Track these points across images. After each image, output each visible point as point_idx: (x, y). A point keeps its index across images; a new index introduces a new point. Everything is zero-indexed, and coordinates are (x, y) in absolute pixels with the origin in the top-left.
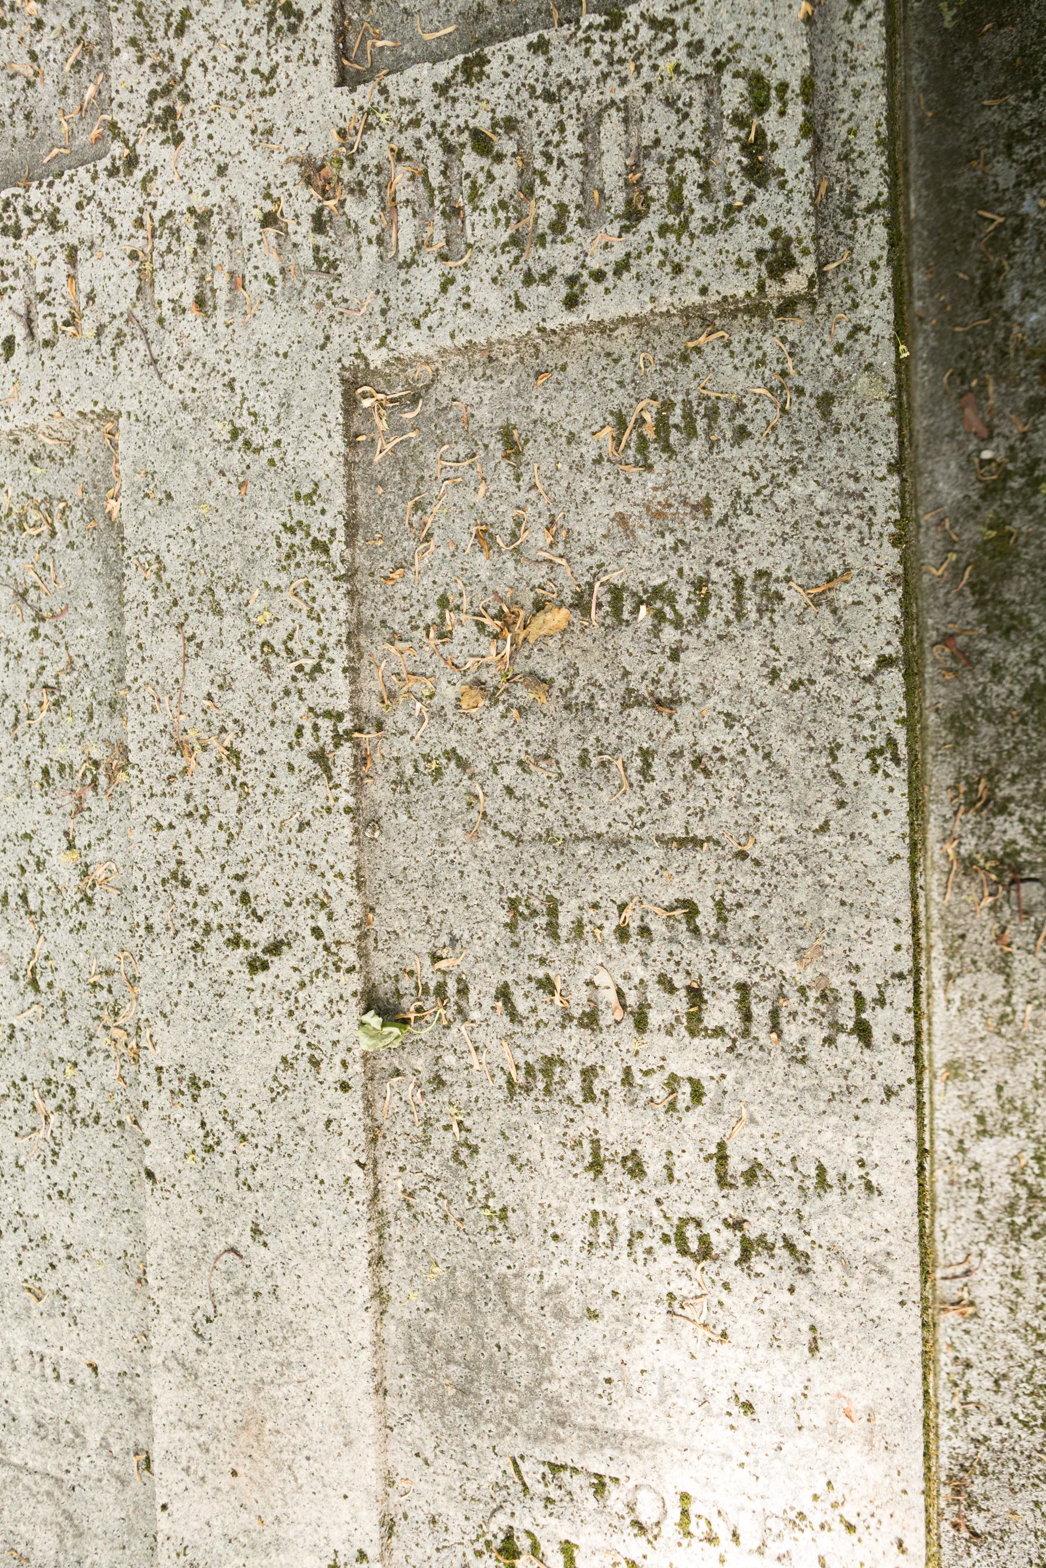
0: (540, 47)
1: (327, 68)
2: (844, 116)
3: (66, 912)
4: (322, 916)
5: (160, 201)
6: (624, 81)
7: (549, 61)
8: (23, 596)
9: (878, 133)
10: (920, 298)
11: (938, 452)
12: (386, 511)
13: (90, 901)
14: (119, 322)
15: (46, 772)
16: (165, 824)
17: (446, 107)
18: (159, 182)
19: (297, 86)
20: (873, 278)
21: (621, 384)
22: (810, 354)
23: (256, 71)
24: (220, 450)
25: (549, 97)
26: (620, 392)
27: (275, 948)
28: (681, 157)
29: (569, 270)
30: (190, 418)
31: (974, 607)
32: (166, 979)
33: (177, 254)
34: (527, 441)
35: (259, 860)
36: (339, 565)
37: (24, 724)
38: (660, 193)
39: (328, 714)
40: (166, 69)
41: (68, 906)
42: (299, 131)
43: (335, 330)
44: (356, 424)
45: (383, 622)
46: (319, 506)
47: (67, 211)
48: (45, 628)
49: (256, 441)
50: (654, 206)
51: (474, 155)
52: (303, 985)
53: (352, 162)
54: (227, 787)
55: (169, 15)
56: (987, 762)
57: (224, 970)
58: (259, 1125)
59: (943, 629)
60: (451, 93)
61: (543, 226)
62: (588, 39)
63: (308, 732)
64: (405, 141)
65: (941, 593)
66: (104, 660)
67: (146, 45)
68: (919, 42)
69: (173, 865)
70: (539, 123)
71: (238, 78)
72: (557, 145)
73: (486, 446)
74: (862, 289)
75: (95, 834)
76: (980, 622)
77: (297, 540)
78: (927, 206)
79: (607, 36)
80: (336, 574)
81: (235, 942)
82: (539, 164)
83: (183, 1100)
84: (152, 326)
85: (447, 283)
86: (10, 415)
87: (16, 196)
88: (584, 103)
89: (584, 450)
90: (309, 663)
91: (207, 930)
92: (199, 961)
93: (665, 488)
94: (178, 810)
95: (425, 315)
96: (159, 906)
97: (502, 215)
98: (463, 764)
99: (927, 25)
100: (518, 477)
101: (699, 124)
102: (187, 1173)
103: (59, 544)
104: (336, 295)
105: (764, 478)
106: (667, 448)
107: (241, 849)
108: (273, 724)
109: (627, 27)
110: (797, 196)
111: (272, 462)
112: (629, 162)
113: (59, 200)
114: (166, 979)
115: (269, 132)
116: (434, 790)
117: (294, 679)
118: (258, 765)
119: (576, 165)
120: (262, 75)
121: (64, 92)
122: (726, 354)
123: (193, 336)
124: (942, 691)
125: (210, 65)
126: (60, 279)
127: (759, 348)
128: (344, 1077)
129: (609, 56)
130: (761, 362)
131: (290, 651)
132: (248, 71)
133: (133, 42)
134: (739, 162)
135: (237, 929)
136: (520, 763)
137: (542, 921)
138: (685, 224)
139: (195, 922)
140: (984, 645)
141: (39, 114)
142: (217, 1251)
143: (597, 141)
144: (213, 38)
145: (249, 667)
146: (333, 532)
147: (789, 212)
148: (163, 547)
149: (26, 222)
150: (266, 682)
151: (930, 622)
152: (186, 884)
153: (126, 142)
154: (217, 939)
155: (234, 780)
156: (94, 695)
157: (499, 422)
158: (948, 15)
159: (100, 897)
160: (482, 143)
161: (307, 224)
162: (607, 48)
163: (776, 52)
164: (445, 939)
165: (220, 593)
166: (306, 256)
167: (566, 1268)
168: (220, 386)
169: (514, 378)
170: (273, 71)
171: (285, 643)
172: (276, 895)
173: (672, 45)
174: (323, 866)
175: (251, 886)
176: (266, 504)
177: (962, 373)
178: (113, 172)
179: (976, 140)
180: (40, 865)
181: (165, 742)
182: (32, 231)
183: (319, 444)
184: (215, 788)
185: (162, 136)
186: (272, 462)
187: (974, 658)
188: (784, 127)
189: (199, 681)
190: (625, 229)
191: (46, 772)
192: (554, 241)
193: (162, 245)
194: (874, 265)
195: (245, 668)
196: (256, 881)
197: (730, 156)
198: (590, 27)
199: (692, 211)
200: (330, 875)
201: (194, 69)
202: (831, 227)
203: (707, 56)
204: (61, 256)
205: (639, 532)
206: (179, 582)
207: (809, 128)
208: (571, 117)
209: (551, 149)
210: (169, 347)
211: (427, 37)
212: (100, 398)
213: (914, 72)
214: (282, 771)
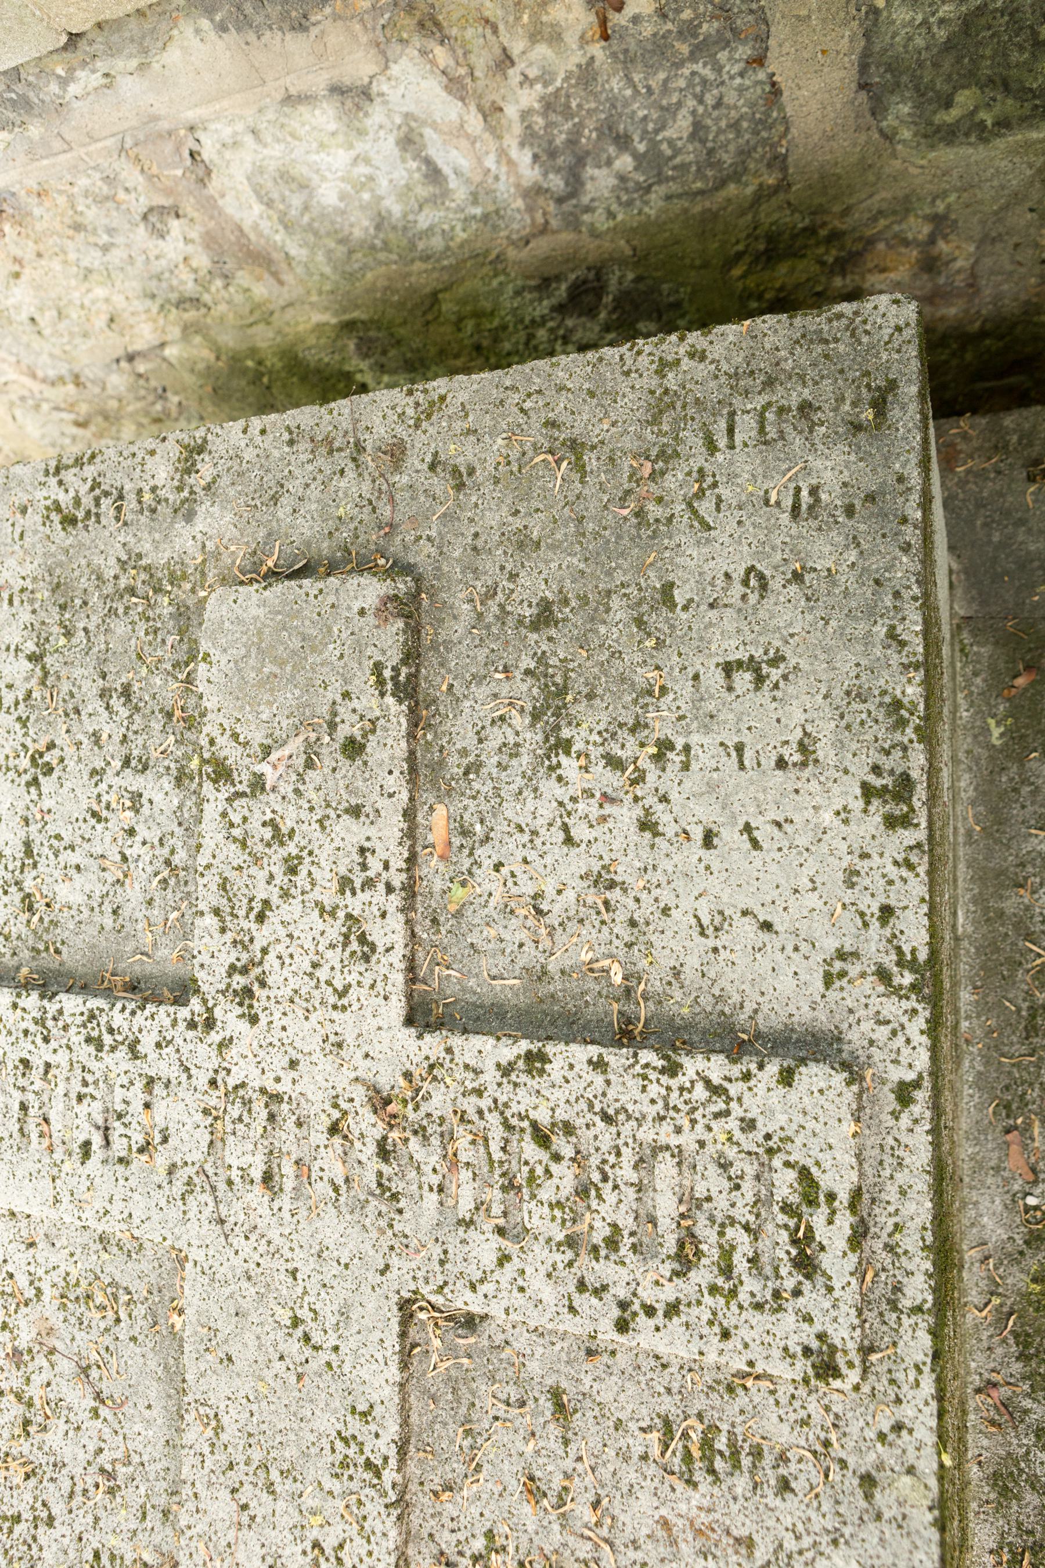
0: (599, 1065)
1: (397, 1008)
2: (891, 1209)
5: (234, 1069)
6: (678, 1130)
7: (608, 1082)
8: (85, 1370)
9: (923, 1239)
10: (968, 1017)
11: (982, 1183)
12: (437, 1426)
14: (190, 1171)
15: (97, 1555)
17: (508, 1088)
18: (233, 1052)
19: (368, 1012)
20: (917, 1381)
21: (669, 1391)
22: (854, 1429)
23: (329, 983)
25: (607, 1118)
26: (666, 1399)
28: (732, 1225)
29: (622, 1293)
30: (253, 1290)
31: (1018, 1359)
33: (247, 1125)
34: (576, 1411)
36: (391, 1492)
37: (79, 1499)
38: (711, 1251)
40: (245, 948)
42: (367, 1055)
43: (394, 1261)
44: (412, 1332)
45: (431, 1535)
46: (373, 1427)
47: (147, 1045)
49: (317, 1338)
50: (704, 1261)
51: (533, 1146)
53: (417, 1108)
55: (251, 900)
56: (1030, 1533)
59: (986, 1375)
60: (513, 1077)
61: (597, 1238)
62: (645, 1077)
64: (470, 1105)
65: (984, 1336)
66: (159, 1466)
67: (228, 918)
68: (968, 752)
70: (596, 1137)
71: (313, 983)
72: (613, 1167)
73: (536, 1400)
74: (905, 1388)
76: (1024, 1378)
77: (351, 1452)
78: (974, 922)
79: (665, 1079)
80: (388, 1501)
82: (596, 1177)
84: (222, 1186)
85: (504, 1259)
87: (102, 1010)
88: (640, 1135)
89: (631, 1441)
93: (709, 1511)
95: (482, 1281)
97: (557, 1213)
99: (975, 736)
100: (566, 1442)
101: (750, 1198)
103: (123, 1331)
104: (398, 1227)
105: (807, 1541)
106: (712, 1471)
109: (682, 1080)
110: (844, 1308)
112: (683, 1209)
113: (140, 1031)
115: (339, 1045)
119: (631, 1193)
120: (335, 990)
121: (150, 902)
122: (772, 1401)
123: (260, 1211)
124: (985, 1442)
125: (288, 961)
126: (137, 1106)
127: (803, 1407)
129: (666, 1099)
130: (804, 1423)
132: (323, 979)
133: (217, 912)
134: (788, 1253)
138: (733, 1293)
140: (1027, 1403)
141: (125, 912)
143: (651, 1171)
144: (290, 936)
146: (386, 1459)
147: (835, 1320)
148: (222, 1407)
149: (108, 1040)
151: (973, 1365)
153: (205, 1001)
157: (549, 1381)
158: (996, 732)
160: (542, 1139)
161: (372, 1148)
162: (664, 1092)
163: (825, 1158)
165: (275, 1475)
166: (371, 1179)
168: (282, 1269)
169: (565, 1345)
170: (347, 988)
171: (335, 1550)
173: (727, 1113)
176: (322, 1405)
177: (1007, 1106)
178: (192, 1025)
179: (1023, 865)
182: (113, 1049)
183: (375, 1366)
185: (239, 1011)
186: (329, 1364)
187: (1017, 1415)
188: (833, 1234)
190: (676, 1274)
191: (97, 1555)
192: (607, 1257)
193: (235, 1111)
194: (919, 1370)
197: (777, 1243)
198: (647, 1066)
199: (741, 1283)
201: (271, 958)
202: (876, 1312)
203: (759, 1135)
204: (139, 1084)
205: (683, 1545)
206: (235, 1446)
207: (858, 1238)
208: (626, 1144)
209: (607, 1168)
210: (234, 1212)
212: (169, 1236)
213: (963, 784)
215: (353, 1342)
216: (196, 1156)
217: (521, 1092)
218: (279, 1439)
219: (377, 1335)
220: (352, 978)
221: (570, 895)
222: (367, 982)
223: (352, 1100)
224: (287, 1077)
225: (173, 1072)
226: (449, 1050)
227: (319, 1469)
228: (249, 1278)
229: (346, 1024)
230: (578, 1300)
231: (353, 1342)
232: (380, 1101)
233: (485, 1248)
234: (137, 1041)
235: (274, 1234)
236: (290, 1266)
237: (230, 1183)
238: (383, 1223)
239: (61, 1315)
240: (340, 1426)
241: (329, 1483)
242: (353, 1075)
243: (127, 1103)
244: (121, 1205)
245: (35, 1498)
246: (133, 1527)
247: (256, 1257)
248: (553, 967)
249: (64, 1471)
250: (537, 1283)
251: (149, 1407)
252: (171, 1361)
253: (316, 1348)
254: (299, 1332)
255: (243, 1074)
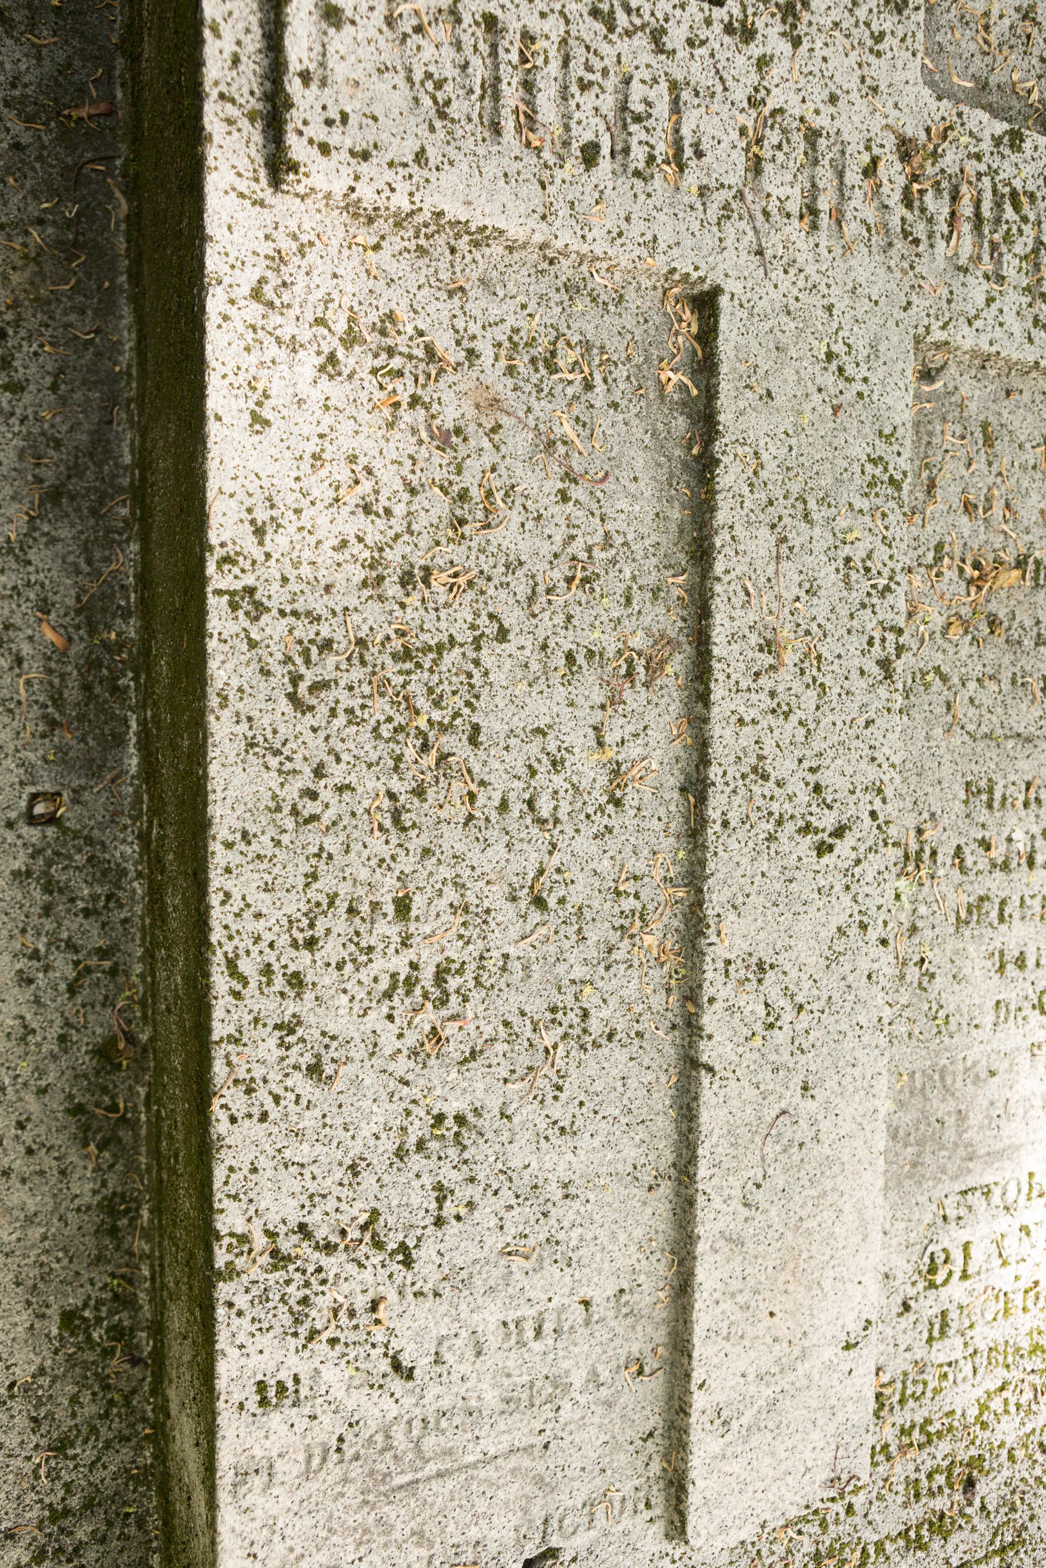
3: (588, 816)
4: (877, 801)
13: (618, 803)
14: (725, 195)
16: (747, 719)
23: (867, 25)
24: (818, 367)
27: (839, 832)
30: (792, 325)
32: (740, 871)
35: (831, 753)
39: (892, 629)
41: (590, 810)
43: (914, 298)
46: (896, 448)
47: (676, 37)
48: (577, 492)
49: (850, 370)
52: (858, 862)
54: (808, 686)
57: (794, 856)
58: (815, 992)
63: (877, 641)
66: (647, 542)
69: (753, 761)
71: (853, 21)
75: (630, 729)
81: (806, 829)
83: (748, 986)
84: (760, 217)
85: (990, 300)
86: (589, 237)
90: (882, 582)
91: (779, 823)
92: (772, 852)
94: (762, 705)
96: (737, 800)
98: (944, 679)
102: (748, 1055)
107: (818, 745)
108: (849, 632)
111: (860, 395)
113: (666, 20)
114: (740, 871)
116: (926, 698)
117: (869, 594)
118: (835, 667)
128: (883, 935)
131: (867, 570)
135: (809, 818)
136: (978, 680)
137: (984, 797)
139: (771, 814)
142: (769, 1120)
145: (833, 577)
150: (845, 593)
152: (765, 777)
154: (790, 827)
155: (814, 680)
156: (634, 578)
157: (982, 418)
159: (631, 799)
164: (926, 815)
165: (812, 504)
167: (976, 1049)
168: (819, 305)
170: (882, 34)
172: (843, 784)
174: (881, 759)
175: (825, 778)
180: (556, 764)
181: (754, 639)
184: (797, 686)
189: (790, 585)
191: (570, 658)
195: (829, 577)
196: (827, 773)
200: (885, 766)
210: (773, 244)
211: (955, 79)
212: (703, 265)
214: (855, 675)
215: (881, 371)
216: (734, 179)
217: (1006, 164)
218: (816, 468)
219: (900, 365)
220: (887, 26)
221: (1007, 22)
222: (900, 34)
223: (882, 146)
224: (827, 110)
225: (705, 79)
226: (960, 115)
227: (851, 493)
228: (789, 313)
229: (879, 70)
230: (1035, 332)
231: (881, 371)
232: (905, 149)
233: (977, 290)
234: (664, 31)
235: (811, 269)
236: (825, 302)
237: (766, 214)
238: (906, 265)
239: (510, 382)
240: (869, 450)
241: (860, 503)
242: (884, 122)
243: (649, 104)
244: (642, 226)
245: (477, 614)
246: (617, 614)
247: (795, 292)
248: (993, 80)
249: (519, 573)
250: (1009, 318)
251: (635, 479)
252: (660, 426)
253: (847, 380)
254: (833, 366)
255: (782, 99)
